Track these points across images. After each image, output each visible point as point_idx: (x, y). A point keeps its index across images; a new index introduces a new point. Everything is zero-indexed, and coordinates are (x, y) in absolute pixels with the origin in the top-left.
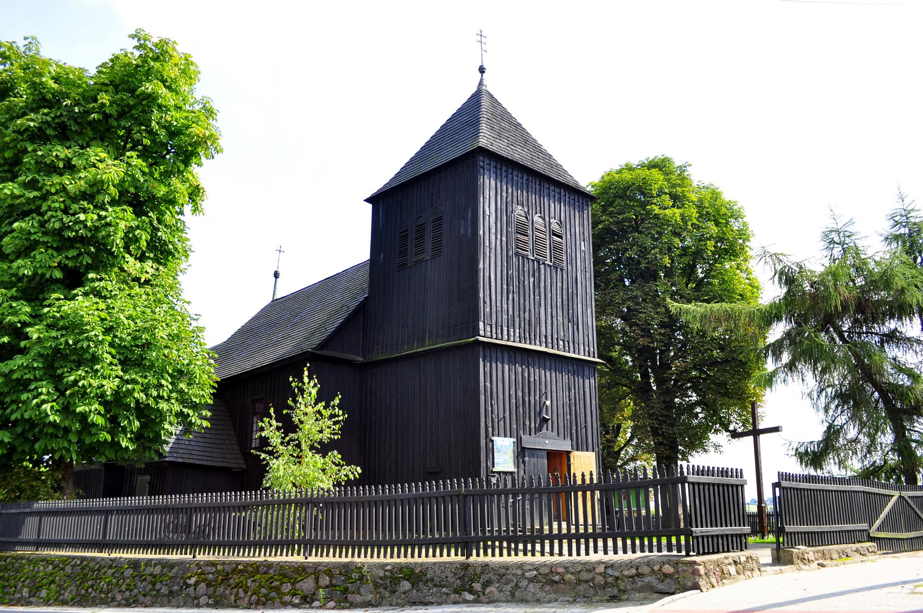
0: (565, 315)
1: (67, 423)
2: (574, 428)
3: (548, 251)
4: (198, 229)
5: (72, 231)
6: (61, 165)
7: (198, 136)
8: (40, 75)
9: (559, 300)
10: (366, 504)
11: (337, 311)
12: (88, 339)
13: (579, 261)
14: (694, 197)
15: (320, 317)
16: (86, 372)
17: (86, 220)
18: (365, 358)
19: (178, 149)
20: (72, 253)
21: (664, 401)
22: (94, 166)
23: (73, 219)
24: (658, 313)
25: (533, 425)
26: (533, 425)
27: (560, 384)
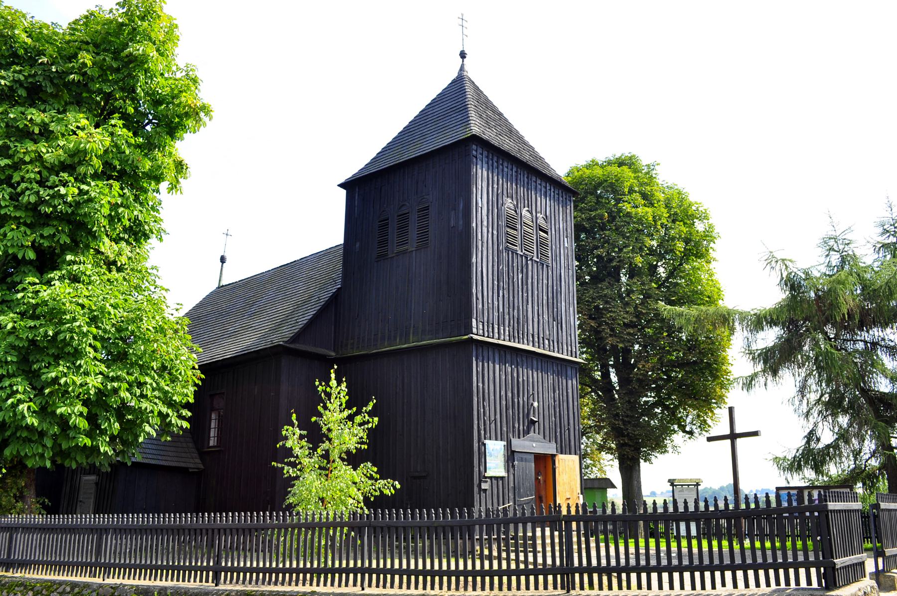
0: (550, 313)
1: (45, 426)
2: (558, 430)
3: (535, 247)
4: (171, 206)
5: (50, 205)
6: (37, 131)
7: (190, 107)
8: (13, 27)
9: (545, 298)
10: (440, 530)
11: (305, 302)
12: (71, 331)
13: (562, 258)
14: (661, 196)
15: (284, 308)
16: (68, 368)
17: (66, 195)
18: (337, 353)
19: (169, 117)
20: (47, 232)
21: (629, 402)
22: (75, 133)
23: (51, 192)
24: (627, 312)
25: (521, 427)
26: (521, 427)
27: (546, 385)
